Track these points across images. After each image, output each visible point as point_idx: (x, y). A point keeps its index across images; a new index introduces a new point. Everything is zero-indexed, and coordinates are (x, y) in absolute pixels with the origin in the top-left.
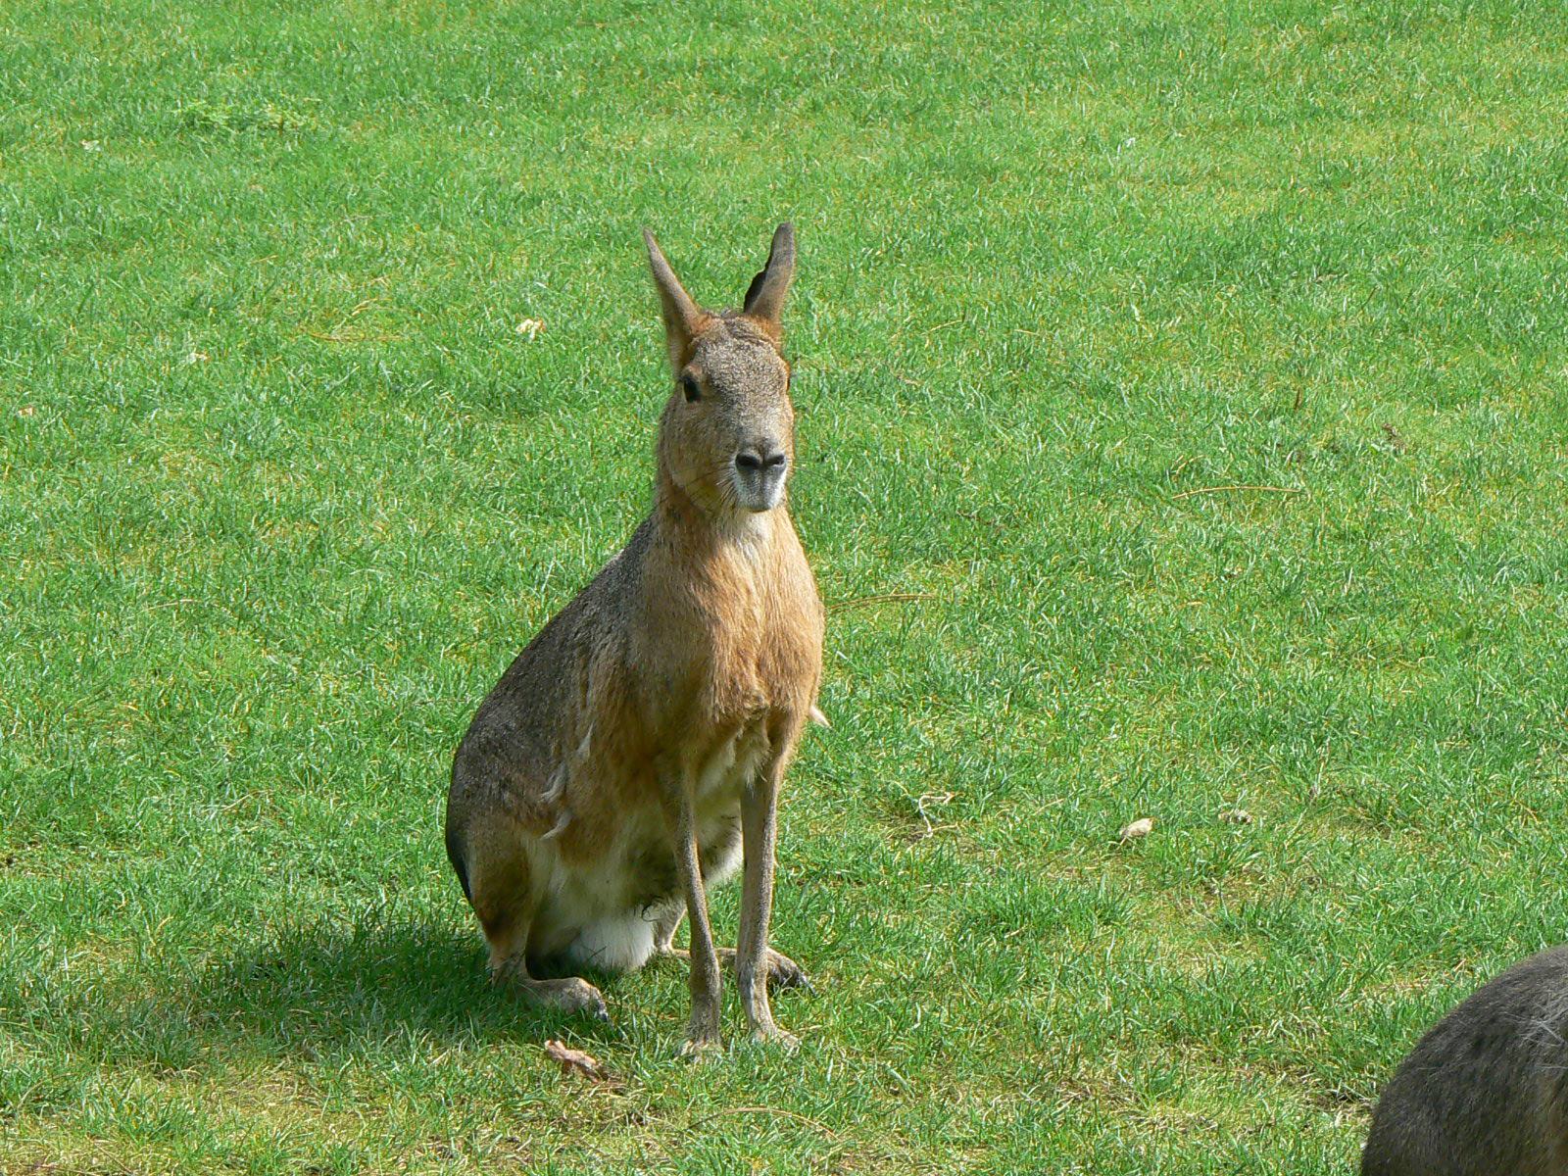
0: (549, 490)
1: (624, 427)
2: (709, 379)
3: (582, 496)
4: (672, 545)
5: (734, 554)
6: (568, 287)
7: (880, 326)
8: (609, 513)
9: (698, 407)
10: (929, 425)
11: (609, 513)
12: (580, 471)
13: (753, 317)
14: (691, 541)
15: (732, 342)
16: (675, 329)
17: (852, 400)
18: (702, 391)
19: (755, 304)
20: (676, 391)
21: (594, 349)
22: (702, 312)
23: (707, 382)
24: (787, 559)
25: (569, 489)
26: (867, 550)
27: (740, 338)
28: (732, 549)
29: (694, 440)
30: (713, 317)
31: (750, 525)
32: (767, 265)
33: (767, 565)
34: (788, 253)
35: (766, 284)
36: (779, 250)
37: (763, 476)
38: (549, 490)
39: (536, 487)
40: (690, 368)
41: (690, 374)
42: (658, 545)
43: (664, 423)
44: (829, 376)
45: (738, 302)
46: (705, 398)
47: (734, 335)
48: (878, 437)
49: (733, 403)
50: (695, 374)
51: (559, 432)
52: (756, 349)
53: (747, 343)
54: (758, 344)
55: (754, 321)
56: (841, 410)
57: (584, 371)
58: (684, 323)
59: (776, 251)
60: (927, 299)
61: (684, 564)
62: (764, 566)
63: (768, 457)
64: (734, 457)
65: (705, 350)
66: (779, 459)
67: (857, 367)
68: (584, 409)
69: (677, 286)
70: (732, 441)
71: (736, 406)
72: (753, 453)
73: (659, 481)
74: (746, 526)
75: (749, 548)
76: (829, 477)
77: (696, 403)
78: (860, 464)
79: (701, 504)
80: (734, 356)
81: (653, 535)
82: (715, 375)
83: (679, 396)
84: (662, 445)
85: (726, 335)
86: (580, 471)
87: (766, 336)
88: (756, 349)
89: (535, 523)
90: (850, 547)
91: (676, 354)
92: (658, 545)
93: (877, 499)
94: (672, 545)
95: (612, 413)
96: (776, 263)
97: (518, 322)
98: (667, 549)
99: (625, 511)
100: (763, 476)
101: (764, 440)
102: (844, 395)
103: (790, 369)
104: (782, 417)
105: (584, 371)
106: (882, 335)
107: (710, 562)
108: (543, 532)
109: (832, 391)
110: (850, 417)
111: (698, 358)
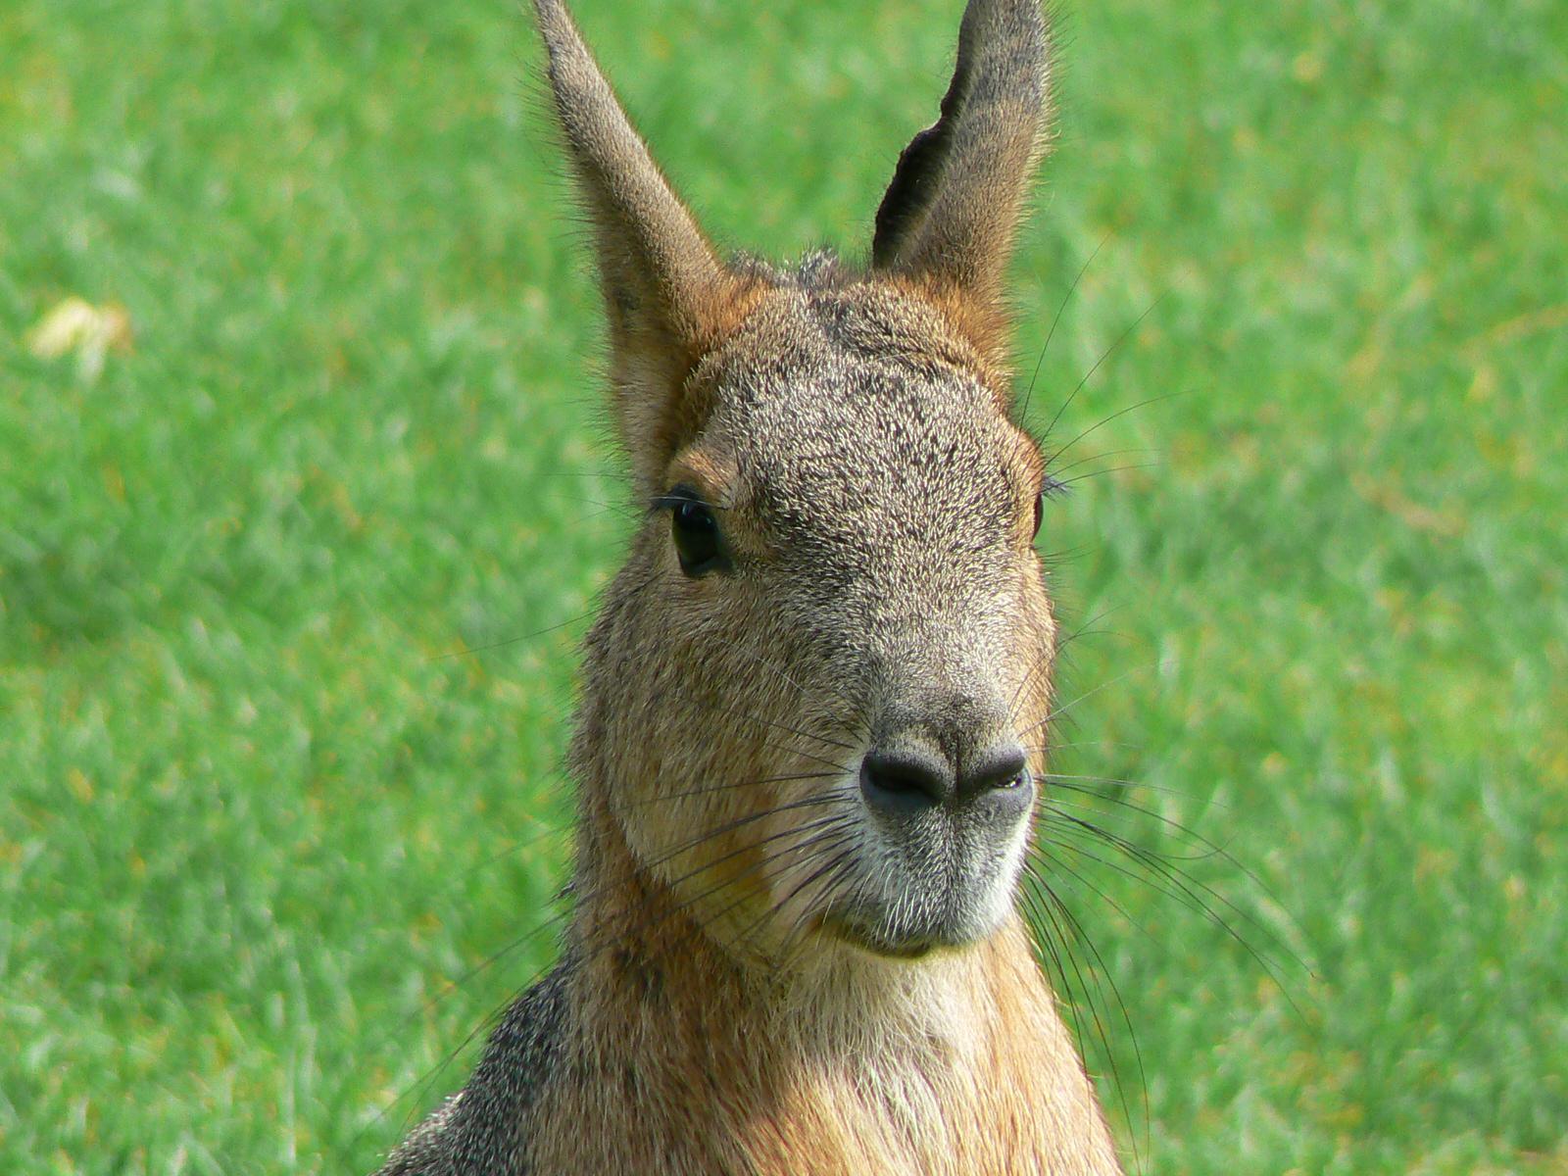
0: (162, 900)
1: (418, 681)
2: (762, 497)
3: (282, 916)
4: (629, 1074)
5: (852, 1106)
6: (215, 192)
7: (1313, 325)
8: (376, 978)
9: (720, 592)
10: (1495, 669)
11: (376, 978)
12: (272, 832)
13: (912, 276)
14: (698, 1060)
15: (840, 365)
16: (639, 323)
17: (1228, 577)
18: (738, 537)
19: (916, 235)
20: (643, 543)
21: (311, 409)
22: (731, 267)
23: (756, 503)
24: (1043, 1128)
25: (234, 893)
26: (1286, 1103)
27: (866, 351)
28: (844, 1088)
29: (711, 702)
30: (771, 284)
31: (907, 1006)
32: (950, 106)
33: (969, 1146)
34: (1024, 57)
35: (952, 167)
36: (997, 48)
37: (959, 830)
38: (162, 900)
39: (118, 889)
40: (695, 459)
41: (697, 479)
42: (581, 1075)
43: (603, 655)
44: (1141, 498)
45: (858, 233)
46: (746, 560)
47: (848, 342)
48: (1314, 713)
49: (846, 576)
50: (712, 479)
51: (186, 696)
52: (924, 390)
53: (893, 371)
54: (931, 374)
55: (918, 293)
56: (1183, 620)
57: (278, 483)
58: (668, 302)
59: (981, 55)
60: (1479, 230)
61: (674, 1141)
62: (959, 1150)
63: (972, 765)
64: (855, 762)
65: (748, 397)
66: (1007, 771)
67: (1238, 466)
68: (279, 616)
69: (644, 173)
70: (845, 706)
71: (859, 587)
72: (919, 749)
73: (590, 861)
74: (893, 1010)
75: (905, 1084)
76: (1146, 852)
77: (714, 580)
78: (1254, 803)
79: (722, 934)
80: (848, 412)
81: (566, 1042)
82: (784, 483)
83: (656, 556)
84: (597, 734)
85: (815, 340)
86: (272, 832)
87: (959, 346)
88: (924, 390)
89: (115, 1016)
90: (1225, 1094)
91: (643, 413)
92: (581, 1075)
93: (1315, 928)
94: (629, 1074)
95: (380, 631)
96: (988, 92)
97: (40, 312)
98: (613, 1089)
99: (432, 972)
100: (959, 830)
101: (957, 703)
102: (1194, 565)
103: (1045, 462)
104: (1016, 627)
105: (278, 483)
106: (1324, 356)
107: (761, 1130)
108: (145, 1048)
109: (1152, 548)
110: (1213, 643)
111: (719, 425)
